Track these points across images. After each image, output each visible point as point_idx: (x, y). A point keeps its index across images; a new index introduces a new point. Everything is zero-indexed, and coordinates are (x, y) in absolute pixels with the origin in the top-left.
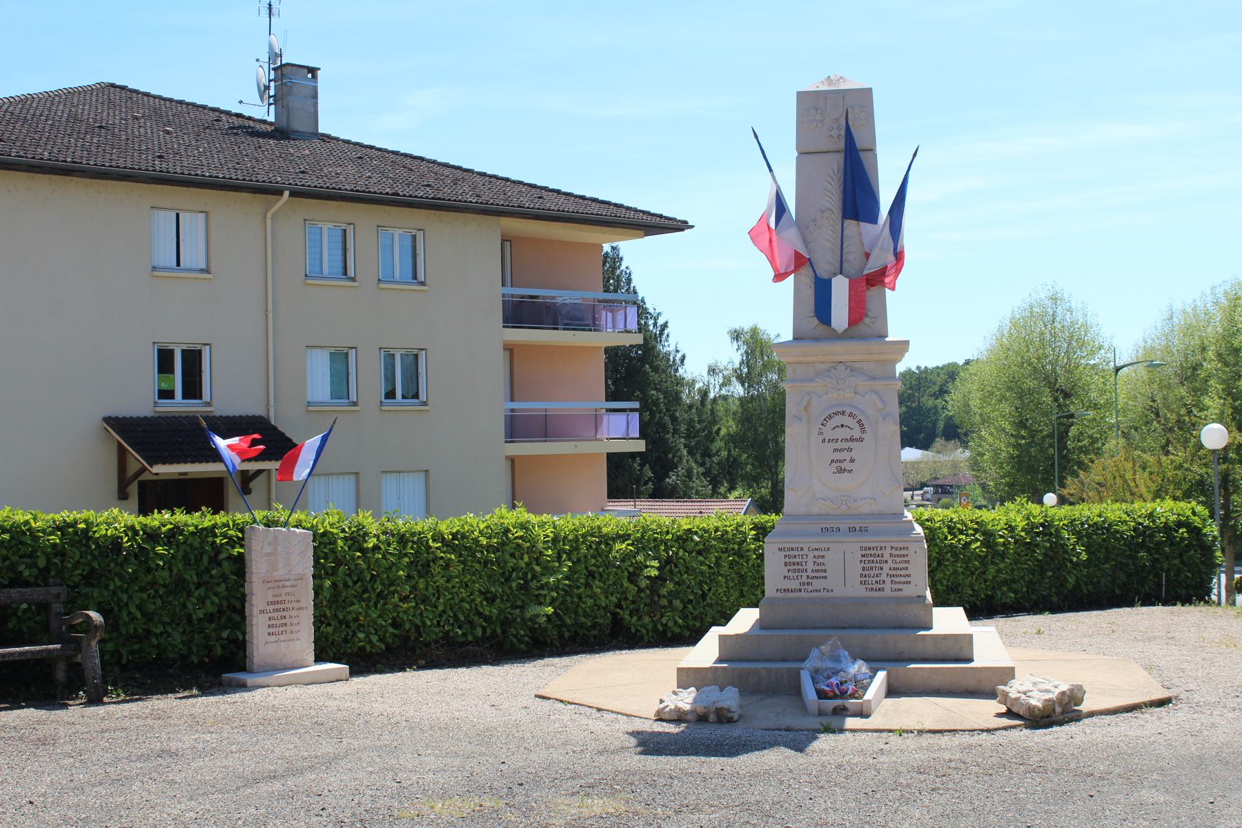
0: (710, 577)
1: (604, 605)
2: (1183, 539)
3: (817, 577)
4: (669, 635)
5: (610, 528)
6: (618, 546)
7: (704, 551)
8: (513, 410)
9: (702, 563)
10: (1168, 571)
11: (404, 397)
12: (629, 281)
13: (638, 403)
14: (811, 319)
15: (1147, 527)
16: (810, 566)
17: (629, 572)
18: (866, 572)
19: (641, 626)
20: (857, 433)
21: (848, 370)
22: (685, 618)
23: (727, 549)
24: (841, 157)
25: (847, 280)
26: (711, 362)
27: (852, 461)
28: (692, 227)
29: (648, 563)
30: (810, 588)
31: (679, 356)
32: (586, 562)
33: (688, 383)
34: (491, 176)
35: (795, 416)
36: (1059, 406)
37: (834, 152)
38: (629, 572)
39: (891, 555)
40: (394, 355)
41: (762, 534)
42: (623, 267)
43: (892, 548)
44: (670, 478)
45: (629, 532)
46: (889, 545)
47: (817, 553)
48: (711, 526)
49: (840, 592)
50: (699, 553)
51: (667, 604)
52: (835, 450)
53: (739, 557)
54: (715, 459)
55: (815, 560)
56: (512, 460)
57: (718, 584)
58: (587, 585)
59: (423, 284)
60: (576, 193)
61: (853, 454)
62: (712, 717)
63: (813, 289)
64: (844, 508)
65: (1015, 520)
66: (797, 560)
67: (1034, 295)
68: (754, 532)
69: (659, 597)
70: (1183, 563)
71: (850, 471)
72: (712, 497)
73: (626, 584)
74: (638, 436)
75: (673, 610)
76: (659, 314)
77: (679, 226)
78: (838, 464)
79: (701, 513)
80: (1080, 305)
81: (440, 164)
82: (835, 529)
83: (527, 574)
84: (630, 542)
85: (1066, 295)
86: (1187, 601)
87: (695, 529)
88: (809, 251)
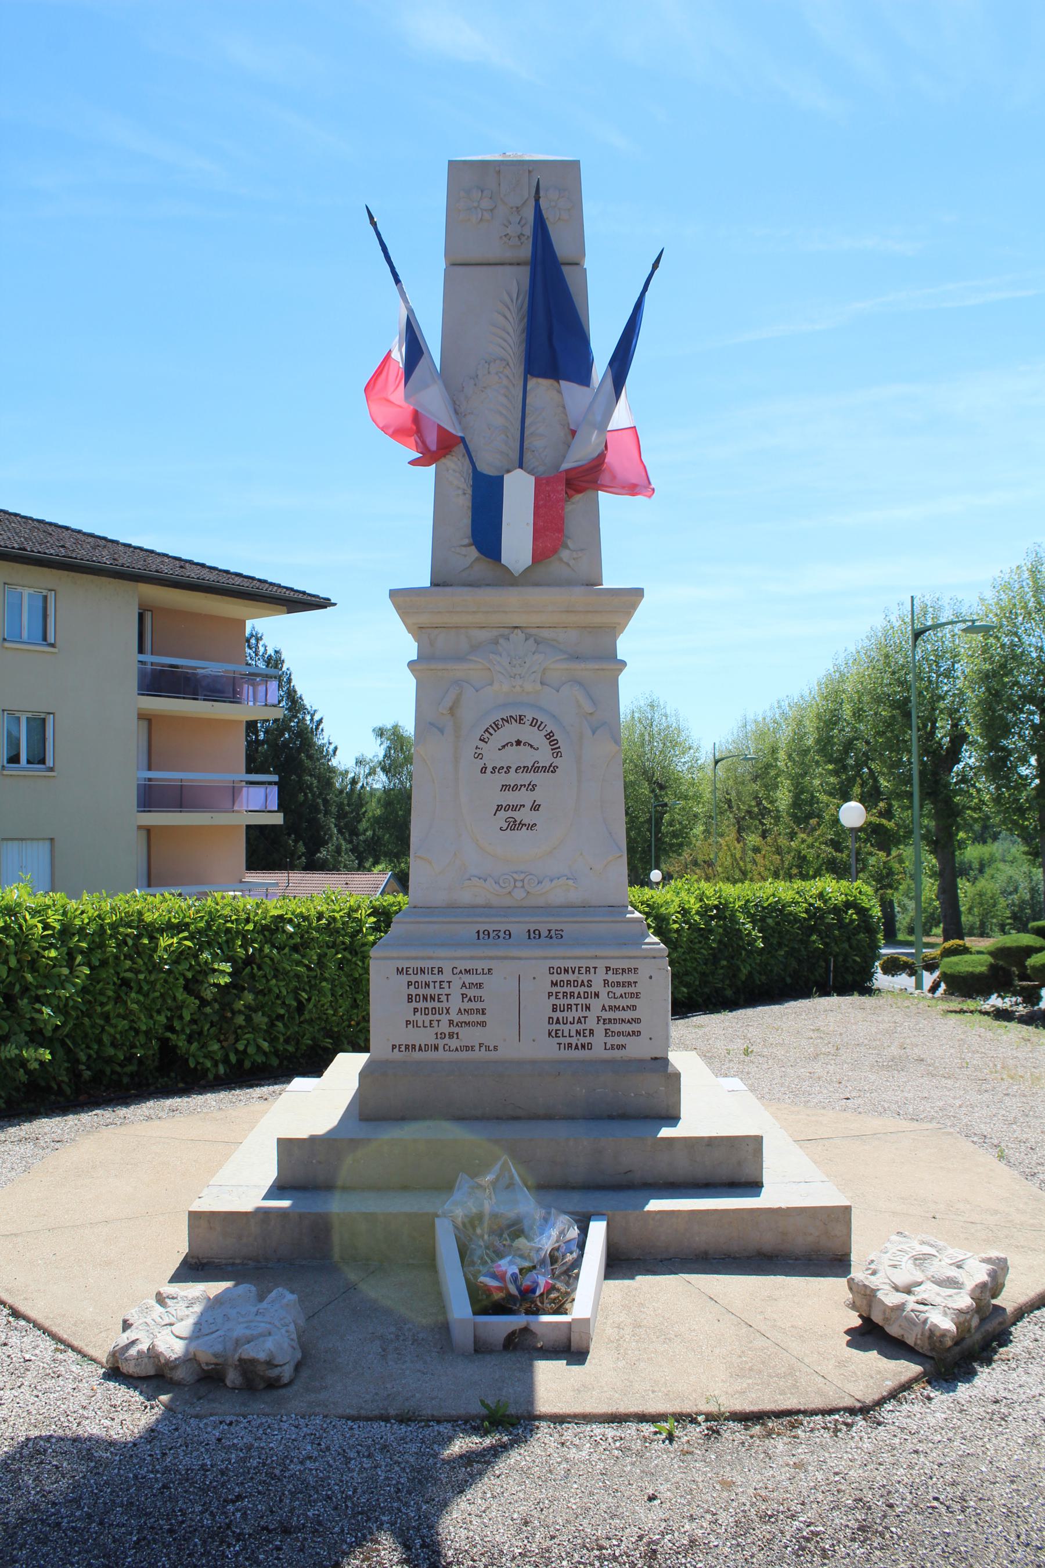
0: (310, 981)
1: (144, 1028)
2: (852, 921)
3: (468, 1024)
4: (247, 1064)
5: (157, 914)
6: (164, 941)
7: (301, 945)
8: (150, 780)
9: (299, 963)
10: (836, 956)
11: (29, 762)
12: (289, 681)
13: (277, 776)
14: (464, 550)
15: (818, 908)
16: (455, 1003)
17: (186, 979)
18: (558, 1014)
19: (205, 1057)
20: (544, 756)
21: (531, 641)
22: (273, 1040)
23: (334, 943)
24: (525, 272)
25: (532, 479)
26: (358, 755)
27: (535, 807)
28: (335, 604)
29: (216, 967)
30: (454, 1043)
31: (332, 747)
32: (117, 965)
33: (341, 774)
34: (136, 548)
35: (431, 724)
36: (656, 796)
37: (511, 264)
38: (186, 979)
39: (606, 982)
40: (19, 718)
41: (383, 921)
42: (284, 669)
43: (608, 969)
44: (321, 853)
45: (187, 920)
46: (601, 965)
47: (468, 979)
48: (313, 912)
49: (512, 1049)
50: (295, 948)
51: (243, 1023)
52: (505, 787)
53: (351, 953)
54: (361, 838)
55: (464, 991)
56: (149, 830)
57: (320, 991)
58: (118, 999)
59: (53, 645)
60: (220, 567)
61: (538, 795)
62: (232, 1377)
63: (469, 496)
64: (519, 894)
65: (689, 902)
66: (431, 991)
67: (635, 702)
68: (372, 919)
69: (233, 1013)
70: (851, 947)
71: (531, 827)
72: (358, 869)
73: (181, 995)
74: (276, 809)
75: (255, 1029)
76: (315, 711)
77: (321, 603)
78: (510, 813)
79: (347, 884)
80: (673, 712)
81: (85, 534)
82: (501, 934)
83: (14, 985)
84: (186, 934)
85: (662, 703)
86: (843, 990)
87: (289, 916)
88: (463, 430)
